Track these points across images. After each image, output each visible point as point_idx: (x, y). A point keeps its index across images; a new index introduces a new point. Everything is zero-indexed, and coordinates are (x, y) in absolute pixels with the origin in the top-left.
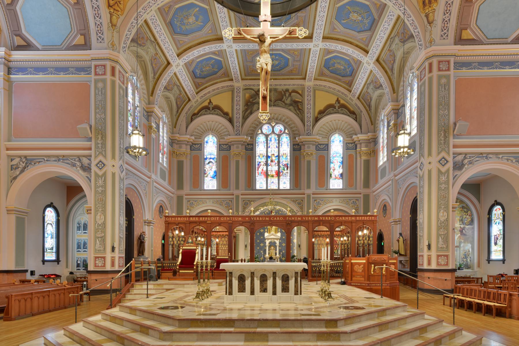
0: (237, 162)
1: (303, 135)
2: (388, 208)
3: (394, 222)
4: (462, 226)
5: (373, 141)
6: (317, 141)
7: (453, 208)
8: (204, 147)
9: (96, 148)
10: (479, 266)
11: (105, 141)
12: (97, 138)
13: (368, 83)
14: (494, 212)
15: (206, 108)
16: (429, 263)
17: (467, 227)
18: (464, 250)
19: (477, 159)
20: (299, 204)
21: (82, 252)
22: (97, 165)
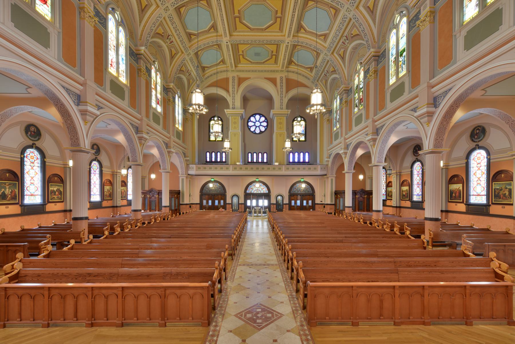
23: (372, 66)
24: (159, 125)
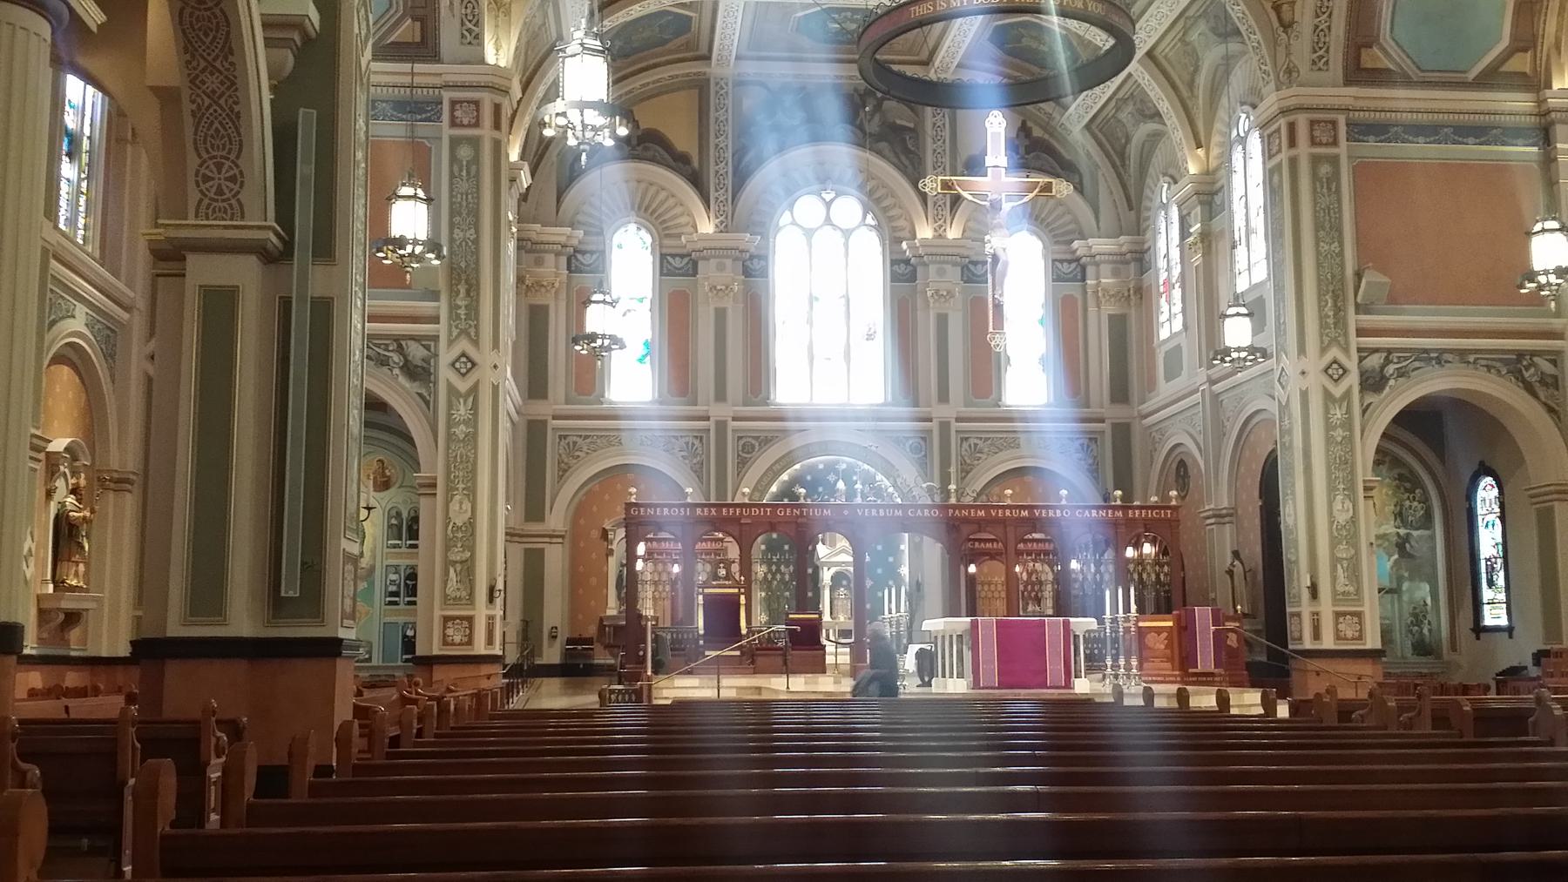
0: (721, 315)
2: (1192, 472)
3: (1215, 516)
4: (1402, 531)
5: (1136, 260)
6: (966, 253)
7: (1366, 489)
9: (450, 317)
10: (1453, 648)
11: (478, 301)
12: (453, 293)
13: (1120, 95)
14: (1481, 494)
17: (1415, 533)
18: (1411, 601)
19: (1417, 364)
21: (402, 606)
22: (453, 365)
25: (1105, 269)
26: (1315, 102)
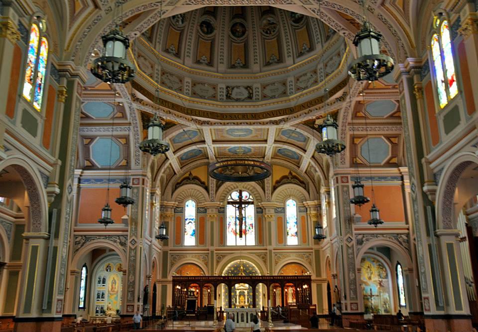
0: (212, 223)
1: (265, 201)
4: (380, 280)
8: (185, 210)
12: (131, 225)
15: (187, 178)
16: (346, 309)
17: (384, 280)
20: (263, 258)
21: (100, 301)
23: (465, 13)
24: (35, 135)
25: (312, 209)
26: (343, 172)
